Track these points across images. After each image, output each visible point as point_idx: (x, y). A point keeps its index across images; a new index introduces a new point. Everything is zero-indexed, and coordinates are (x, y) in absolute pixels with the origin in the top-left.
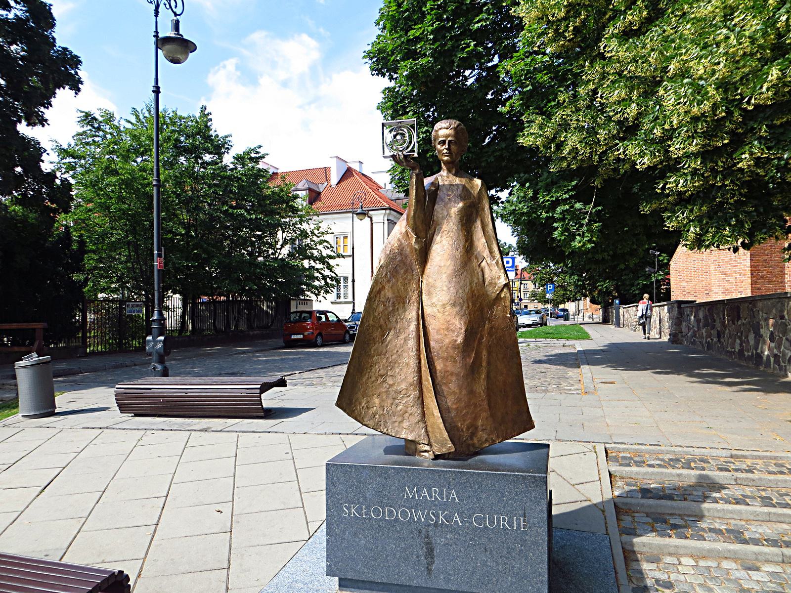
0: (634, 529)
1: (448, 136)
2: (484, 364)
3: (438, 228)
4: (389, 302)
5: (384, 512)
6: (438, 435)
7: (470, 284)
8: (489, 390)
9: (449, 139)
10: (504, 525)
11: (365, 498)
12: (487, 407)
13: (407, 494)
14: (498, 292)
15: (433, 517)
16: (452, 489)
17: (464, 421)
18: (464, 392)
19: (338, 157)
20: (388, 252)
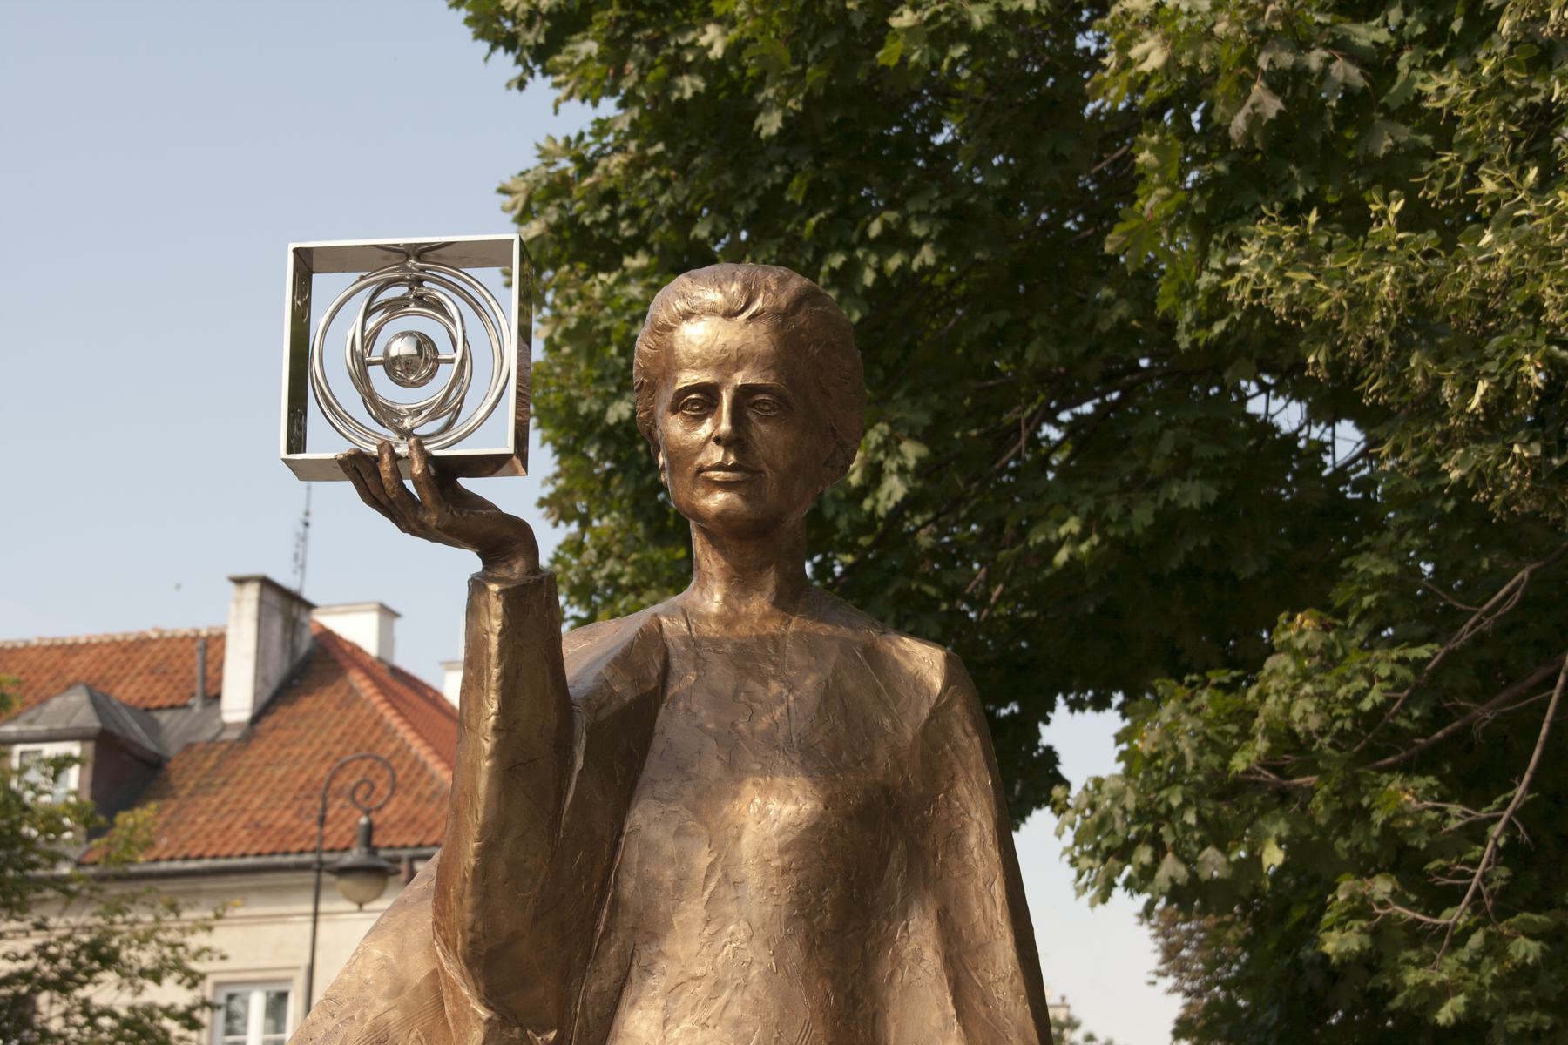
1: (729, 362)
9: (739, 379)
19: (266, 583)
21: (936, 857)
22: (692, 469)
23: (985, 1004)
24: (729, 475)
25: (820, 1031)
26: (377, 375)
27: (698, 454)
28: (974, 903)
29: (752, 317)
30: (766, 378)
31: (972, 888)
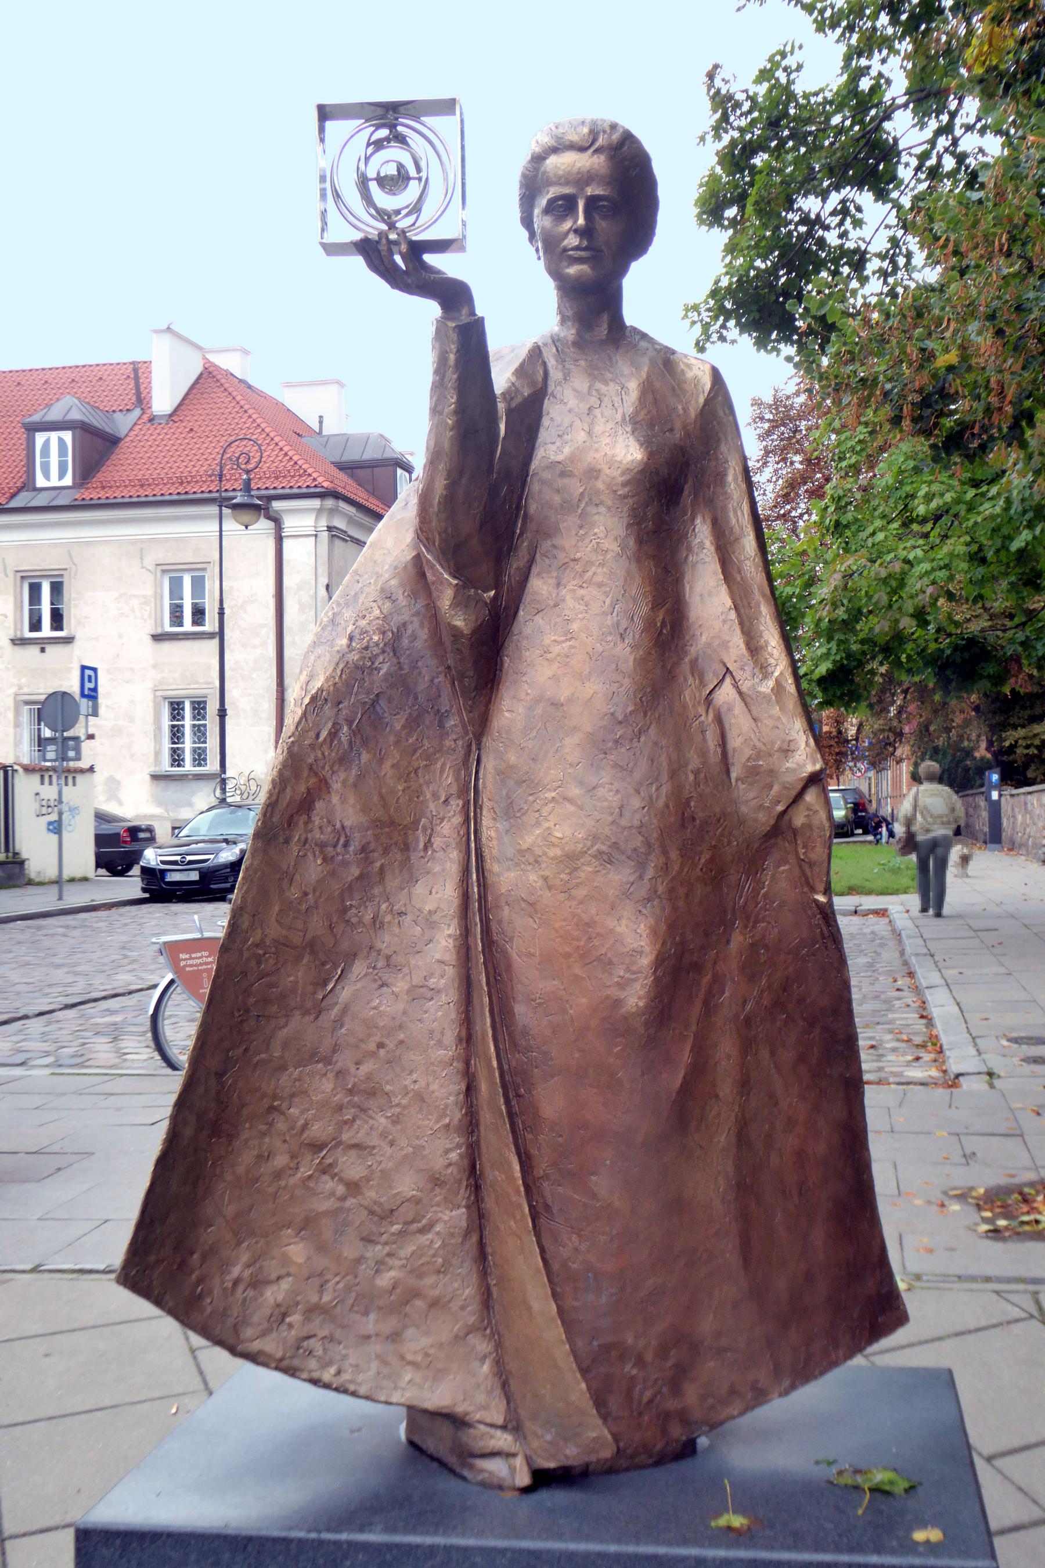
1: (584, 179)
4: (346, 845)
9: (589, 191)
14: (780, 808)
21: (709, 488)
22: (560, 249)
23: (739, 572)
24: (583, 254)
25: (648, 589)
26: (373, 186)
28: (731, 515)
29: (596, 151)
30: (605, 190)
31: (730, 506)
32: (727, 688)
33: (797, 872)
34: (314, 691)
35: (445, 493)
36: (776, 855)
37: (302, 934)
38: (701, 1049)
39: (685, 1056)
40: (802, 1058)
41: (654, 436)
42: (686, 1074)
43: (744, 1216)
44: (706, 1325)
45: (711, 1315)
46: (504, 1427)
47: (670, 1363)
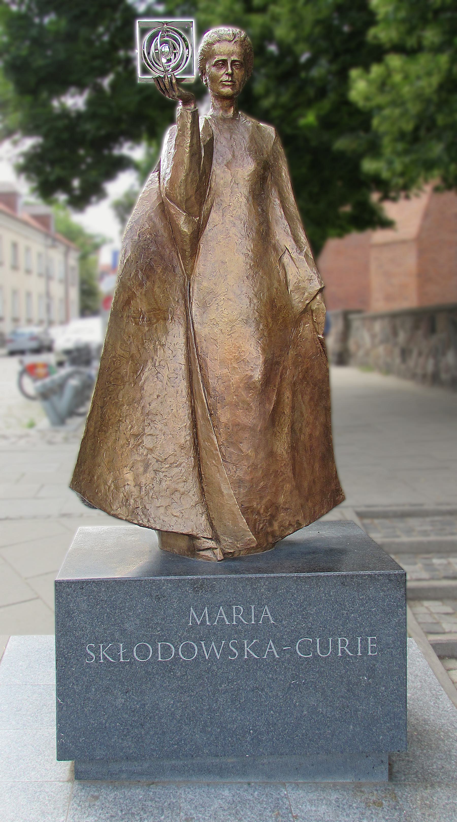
0: (438, 623)
1: (231, 54)
2: (287, 411)
3: (217, 200)
4: (143, 318)
5: (155, 651)
6: (230, 524)
7: (268, 289)
8: (293, 448)
9: (233, 58)
10: (343, 651)
11: (123, 631)
12: (291, 475)
13: (194, 619)
14: (307, 302)
15: (235, 650)
16: (264, 605)
17: (261, 498)
18: (262, 455)
20: (137, 238)
24: (229, 83)
27: (220, 78)
28: (285, 188)
32: (287, 255)
33: (312, 326)
34: (127, 257)
35: (35, 185)
36: (305, 320)
37: (129, 353)
38: (279, 394)
39: (274, 398)
40: (311, 399)
41: (258, 157)
42: (274, 404)
43: (293, 458)
44: (282, 499)
45: (283, 496)
46: (211, 539)
47: (269, 513)
